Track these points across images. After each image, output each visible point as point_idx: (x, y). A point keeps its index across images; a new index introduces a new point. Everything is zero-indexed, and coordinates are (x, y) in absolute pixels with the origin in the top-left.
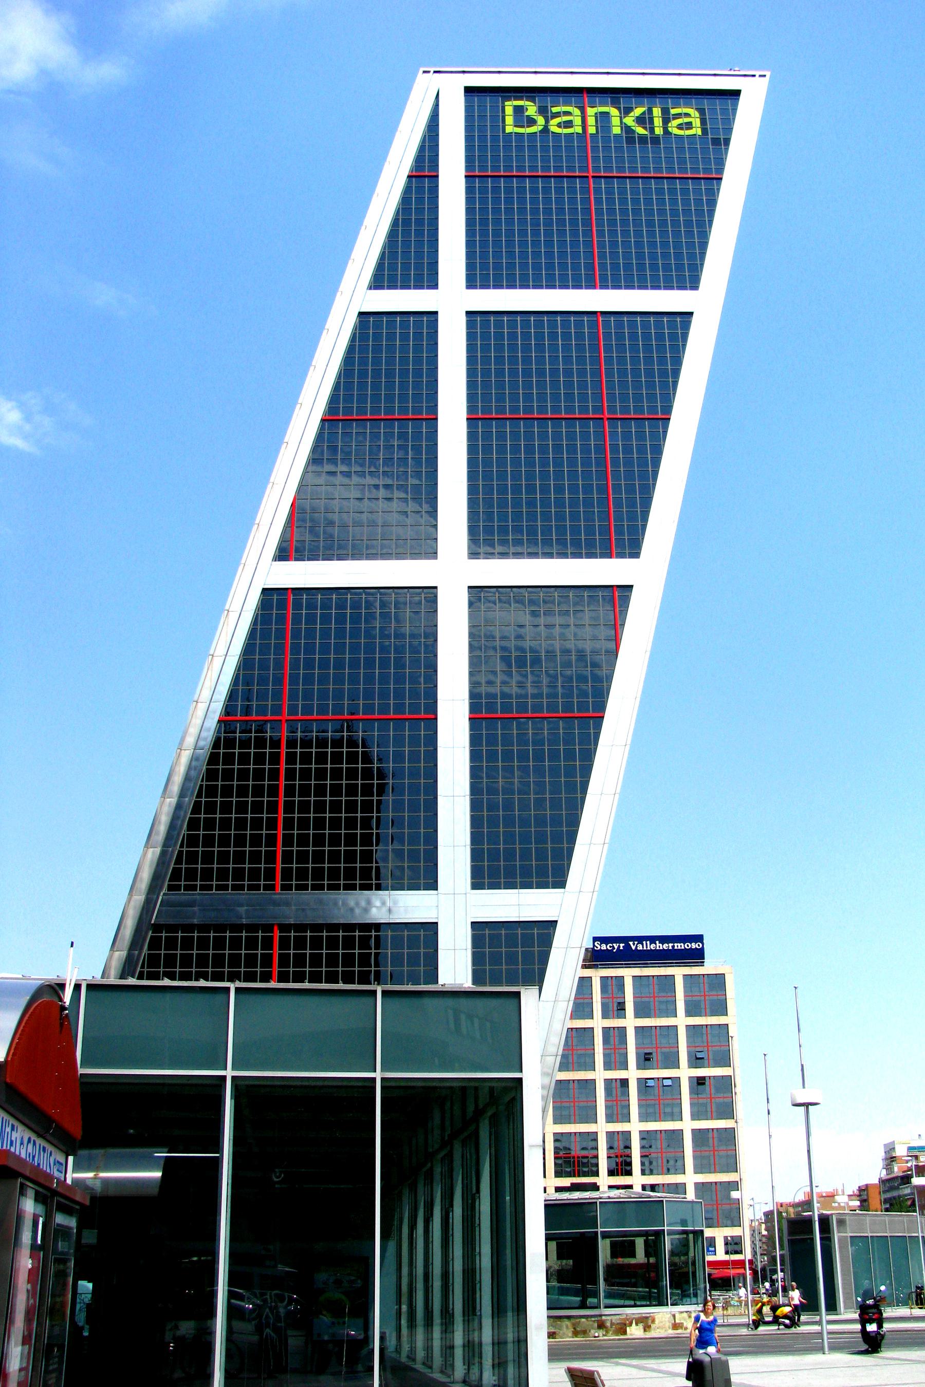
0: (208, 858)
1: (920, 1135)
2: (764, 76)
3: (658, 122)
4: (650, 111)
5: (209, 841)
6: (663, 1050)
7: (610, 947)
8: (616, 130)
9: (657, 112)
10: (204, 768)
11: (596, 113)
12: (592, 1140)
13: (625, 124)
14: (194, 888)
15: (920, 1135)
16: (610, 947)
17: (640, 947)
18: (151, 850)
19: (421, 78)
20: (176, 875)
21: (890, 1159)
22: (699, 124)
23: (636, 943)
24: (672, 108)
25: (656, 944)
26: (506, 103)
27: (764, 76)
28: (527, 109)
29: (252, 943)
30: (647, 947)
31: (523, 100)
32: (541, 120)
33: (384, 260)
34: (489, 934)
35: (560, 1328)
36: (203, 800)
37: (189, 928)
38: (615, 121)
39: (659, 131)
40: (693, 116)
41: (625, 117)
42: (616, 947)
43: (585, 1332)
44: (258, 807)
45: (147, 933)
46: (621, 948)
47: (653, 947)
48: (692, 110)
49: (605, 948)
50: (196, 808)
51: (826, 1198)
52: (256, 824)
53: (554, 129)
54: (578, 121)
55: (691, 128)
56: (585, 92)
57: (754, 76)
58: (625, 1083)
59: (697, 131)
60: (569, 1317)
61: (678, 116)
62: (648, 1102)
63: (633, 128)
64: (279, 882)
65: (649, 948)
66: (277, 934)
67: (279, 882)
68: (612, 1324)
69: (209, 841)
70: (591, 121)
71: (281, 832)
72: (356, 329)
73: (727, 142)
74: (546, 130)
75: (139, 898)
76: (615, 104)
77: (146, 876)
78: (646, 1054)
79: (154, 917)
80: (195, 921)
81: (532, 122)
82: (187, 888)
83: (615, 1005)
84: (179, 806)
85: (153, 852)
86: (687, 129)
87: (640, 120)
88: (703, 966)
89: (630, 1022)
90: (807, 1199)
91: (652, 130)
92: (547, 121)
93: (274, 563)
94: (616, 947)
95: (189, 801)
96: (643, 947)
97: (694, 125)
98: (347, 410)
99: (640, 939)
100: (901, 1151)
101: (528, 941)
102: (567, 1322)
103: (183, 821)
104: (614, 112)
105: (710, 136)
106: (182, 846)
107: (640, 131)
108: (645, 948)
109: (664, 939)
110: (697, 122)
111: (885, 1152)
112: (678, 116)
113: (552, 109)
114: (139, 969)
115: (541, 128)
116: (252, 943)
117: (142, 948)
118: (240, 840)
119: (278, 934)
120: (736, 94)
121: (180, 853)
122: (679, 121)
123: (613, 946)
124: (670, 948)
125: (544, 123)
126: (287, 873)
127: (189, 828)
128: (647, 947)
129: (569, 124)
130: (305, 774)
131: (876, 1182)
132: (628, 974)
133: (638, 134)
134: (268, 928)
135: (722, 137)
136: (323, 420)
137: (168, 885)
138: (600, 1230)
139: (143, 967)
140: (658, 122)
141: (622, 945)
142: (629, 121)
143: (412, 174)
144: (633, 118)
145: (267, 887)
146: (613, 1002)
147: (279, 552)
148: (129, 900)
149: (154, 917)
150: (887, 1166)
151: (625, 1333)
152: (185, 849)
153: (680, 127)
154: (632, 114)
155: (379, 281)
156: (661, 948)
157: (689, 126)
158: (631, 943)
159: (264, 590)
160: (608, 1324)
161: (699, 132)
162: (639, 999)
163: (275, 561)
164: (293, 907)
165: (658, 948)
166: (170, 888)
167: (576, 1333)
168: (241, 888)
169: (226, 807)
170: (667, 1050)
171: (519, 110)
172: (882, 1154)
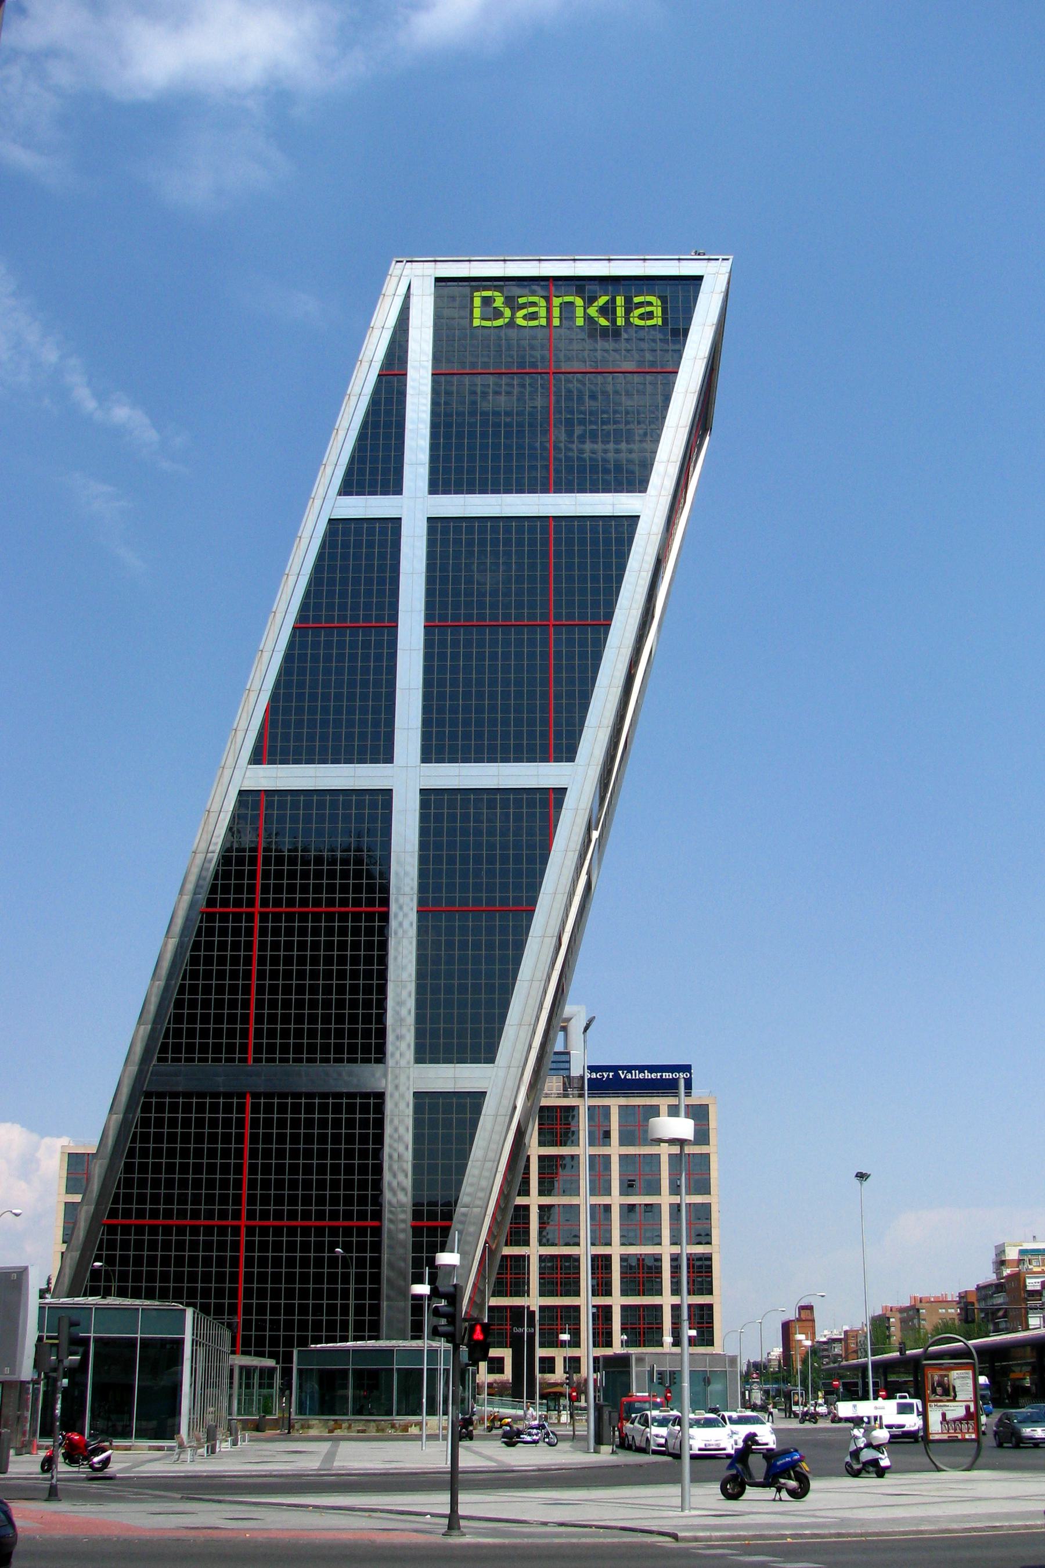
0: (191, 1034)
1: (1034, 1237)
2: (727, 259)
3: (620, 312)
4: (613, 300)
5: (192, 1018)
6: (647, 1177)
7: (600, 1075)
8: (580, 322)
9: (620, 300)
10: (188, 954)
11: (561, 304)
12: (656, 1236)
13: (589, 315)
14: (179, 1060)
15: (1034, 1237)
16: (600, 1075)
17: (629, 1076)
18: (143, 1027)
19: (396, 269)
20: (164, 1049)
21: (1001, 1263)
22: (660, 314)
23: (625, 1072)
24: (635, 296)
25: (644, 1073)
26: (475, 294)
27: (727, 259)
28: (495, 300)
29: (228, 1108)
30: (635, 1076)
31: (491, 290)
32: (508, 313)
33: (367, 429)
34: (429, 1102)
35: (369, 1428)
36: (203, 939)
37: (175, 1095)
38: (579, 312)
39: (620, 322)
40: (655, 304)
41: (588, 307)
42: (606, 1076)
43: (383, 1430)
44: (234, 989)
45: (140, 1099)
46: (611, 1077)
47: (641, 1076)
48: (655, 298)
49: (595, 1077)
50: (182, 990)
51: (934, 1304)
52: (233, 1004)
53: (521, 322)
54: (543, 312)
55: (652, 319)
56: (551, 280)
57: (718, 259)
58: (608, 1208)
59: (658, 321)
60: (374, 1421)
61: (640, 305)
62: (630, 1227)
63: (596, 319)
64: (251, 1056)
65: (637, 1077)
66: (249, 1101)
67: (251, 1056)
68: (400, 1426)
69: (192, 1018)
70: (556, 312)
71: (253, 1012)
72: (219, 864)
73: (686, 332)
74: (511, 324)
75: (133, 1069)
76: (580, 292)
77: (139, 1049)
78: (630, 1181)
79: (145, 1086)
80: (180, 1089)
81: (498, 314)
82: (174, 1060)
83: (602, 1132)
84: (166, 988)
85: (145, 1028)
86: (648, 319)
87: (603, 311)
88: (690, 1096)
89: (615, 1150)
90: (913, 1303)
91: (614, 321)
92: (513, 314)
93: (339, 497)
94: (606, 1076)
95: (203, 897)
96: (632, 1076)
97: (655, 315)
98: (317, 619)
99: (629, 1069)
100: (1012, 1254)
101: (461, 1109)
102: (373, 1424)
103: (170, 1002)
104: (579, 302)
105: (670, 327)
106: (169, 1023)
107: (603, 322)
108: (634, 1077)
109: (652, 1069)
110: (658, 311)
111: (996, 1255)
112: (640, 305)
113: (519, 299)
114: (133, 1130)
115: (507, 320)
116: (228, 1108)
117: (135, 1112)
118: (219, 1019)
119: (250, 1101)
120: (700, 278)
121: (168, 1029)
122: (641, 310)
123: (603, 1075)
124: (659, 1077)
125: (510, 316)
126: (258, 1049)
127: (175, 1008)
128: (635, 1076)
129: (533, 316)
130: (275, 960)
131: (974, 1289)
132: (614, 1103)
133: (601, 325)
134: (242, 1095)
135: (681, 327)
136: (294, 628)
137: (158, 1057)
138: (395, 1367)
139: (136, 1127)
140: (620, 312)
141: (611, 1074)
142: (593, 311)
143: (383, 373)
144: (596, 308)
145: (241, 1060)
146: (599, 1131)
147: (254, 756)
148: (124, 1071)
149: (145, 1086)
150: (997, 1270)
151: (407, 1431)
152: (171, 1026)
153: (641, 317)
154: (596, 304)
155: (349, 487)
156: (650, 1077)
157: (650, 315)
158: (620, 1072)
159: (330, 520)
160: (397, 1426)
161: (660, 323)
162: (625, 1128)
163: (340, 495)
164: (263, 1078)
165: (646, 1077)
166: (160, 1060)
167: (378, 1431)
168: (219, 1060)
169: (207, 990)
170: (650, 1177)
171: (487, 301)
172: (992, 1256)
